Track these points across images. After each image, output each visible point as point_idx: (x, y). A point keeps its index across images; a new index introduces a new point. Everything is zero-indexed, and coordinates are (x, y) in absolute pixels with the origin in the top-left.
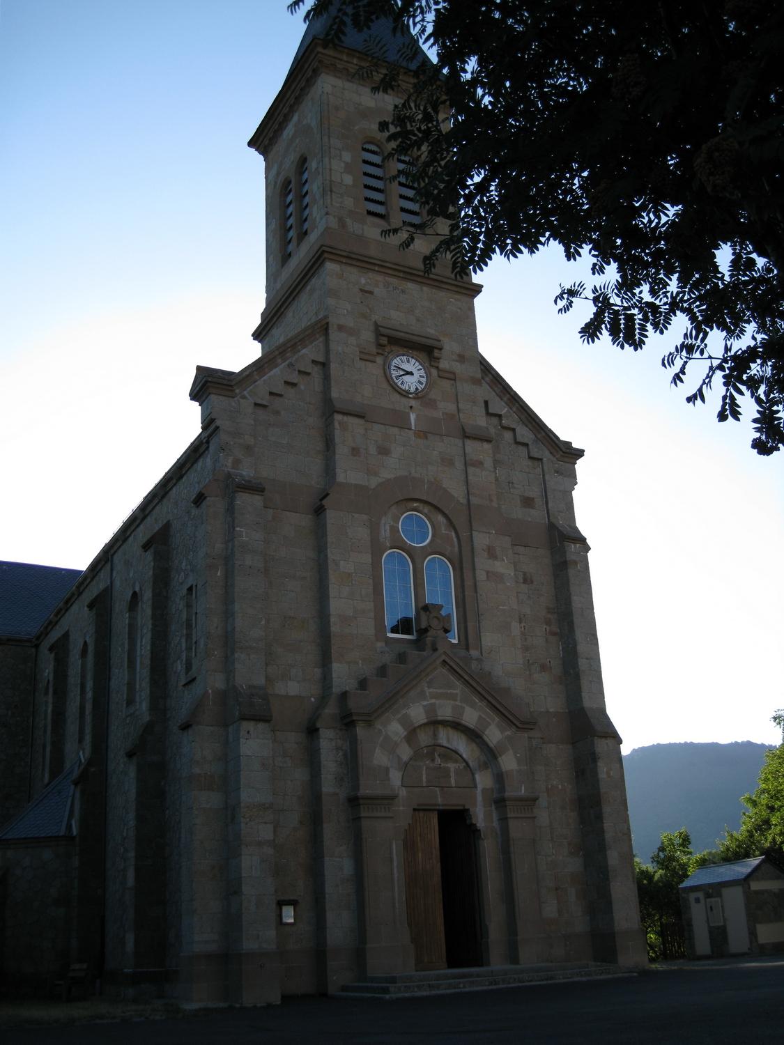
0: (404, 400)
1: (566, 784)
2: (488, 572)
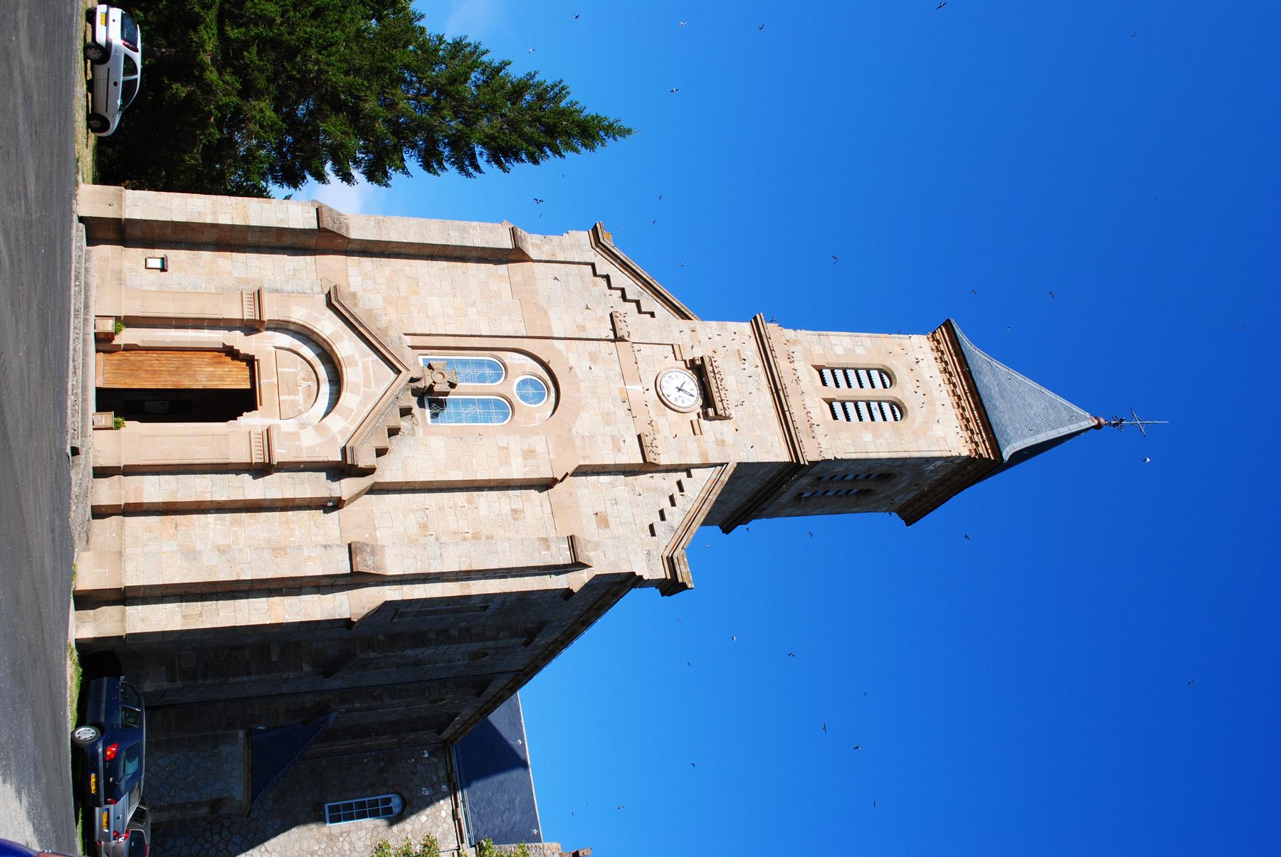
2: (507, 448)
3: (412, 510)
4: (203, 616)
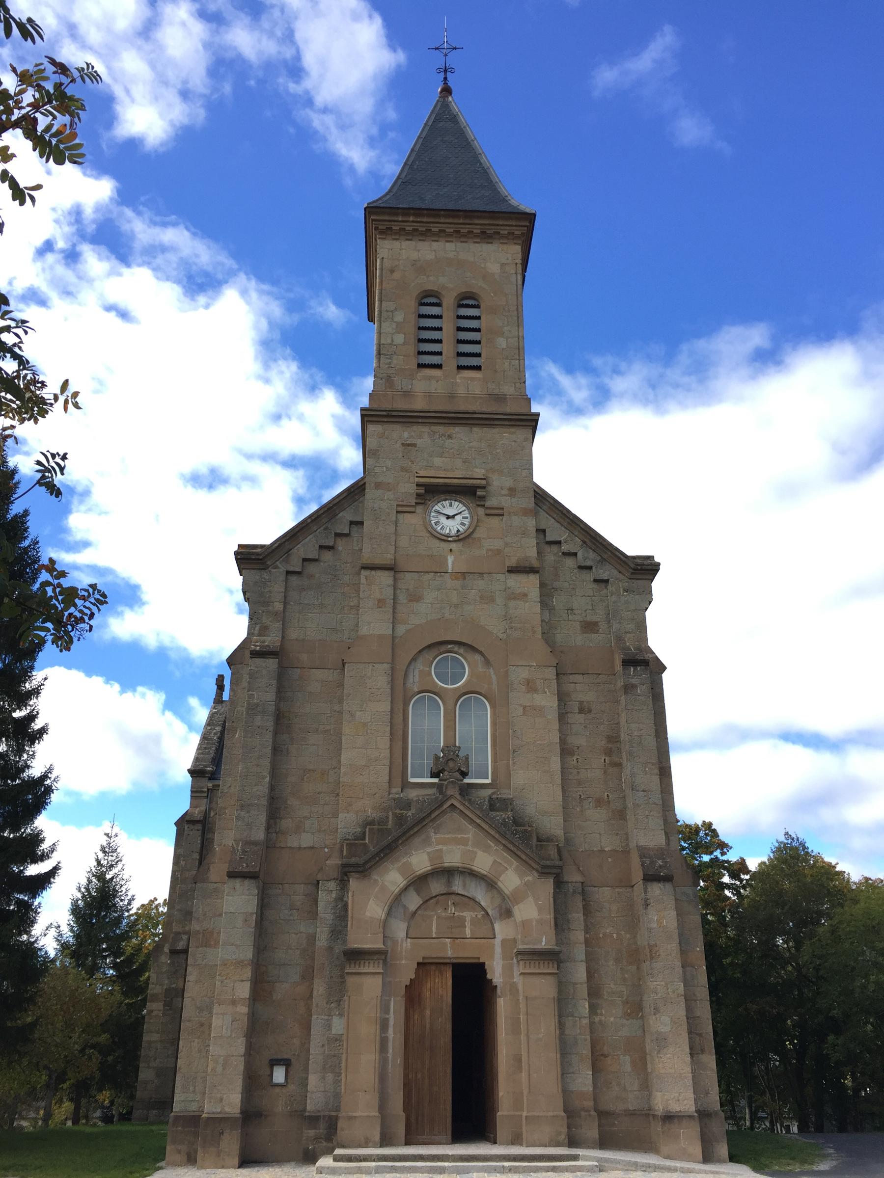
0: (443, 544)
1: (623, 933)
2: (525, 707)
3: (582, 811)
4: (701, 1032)
